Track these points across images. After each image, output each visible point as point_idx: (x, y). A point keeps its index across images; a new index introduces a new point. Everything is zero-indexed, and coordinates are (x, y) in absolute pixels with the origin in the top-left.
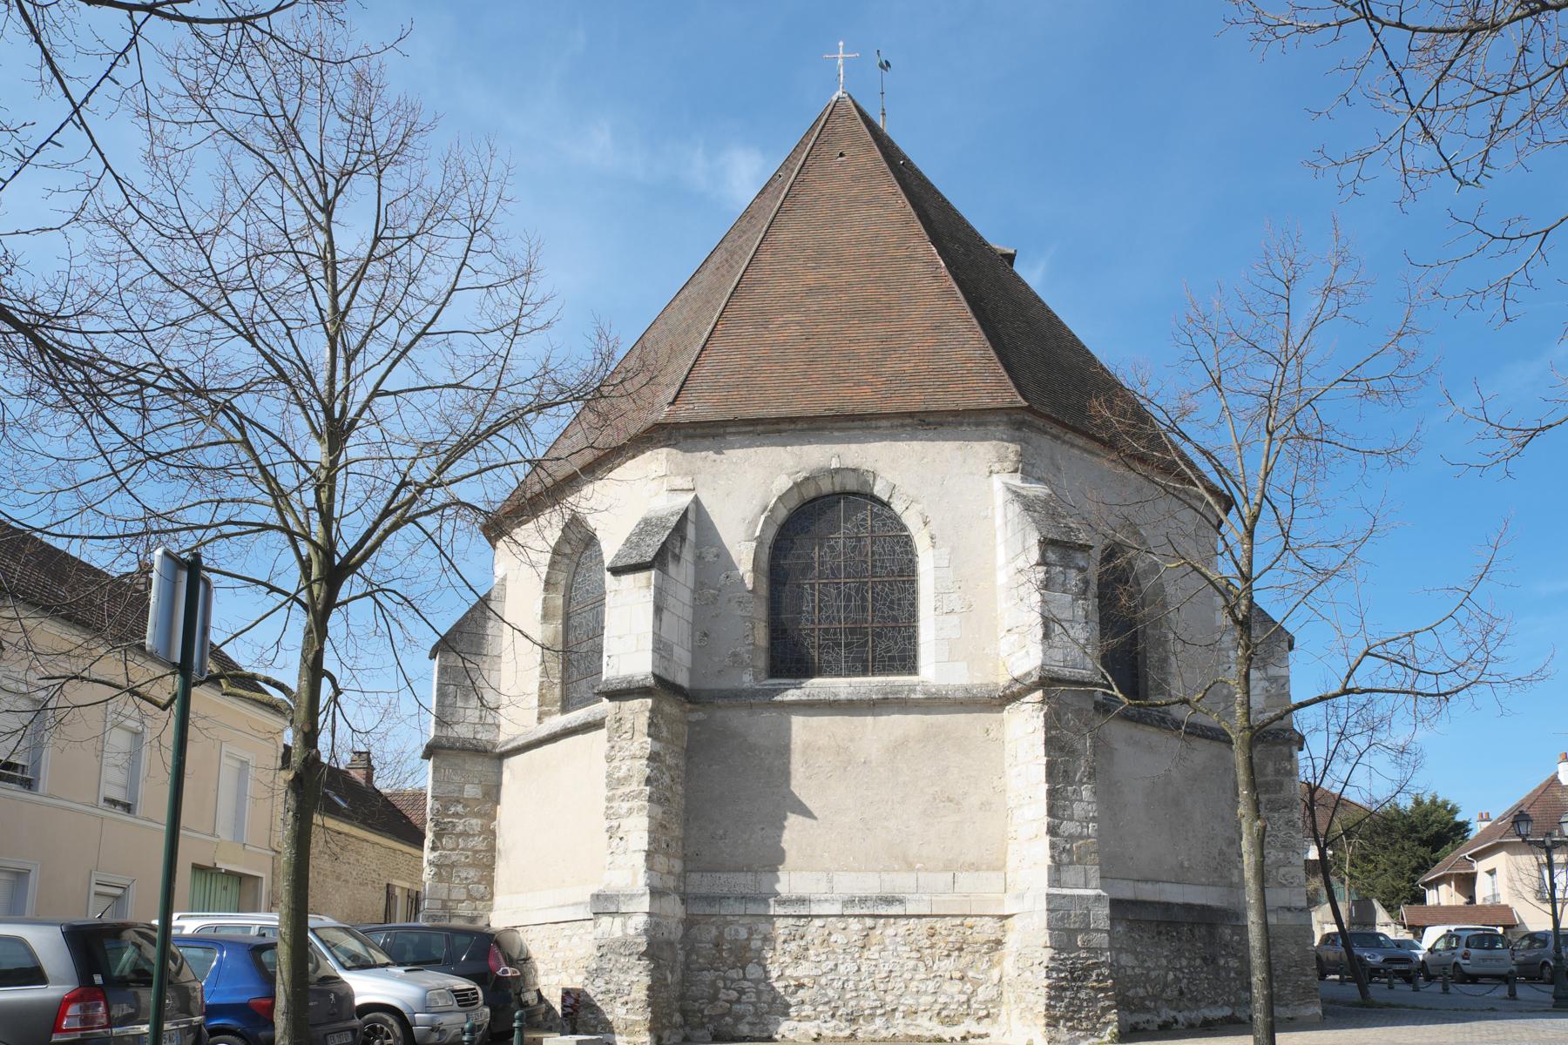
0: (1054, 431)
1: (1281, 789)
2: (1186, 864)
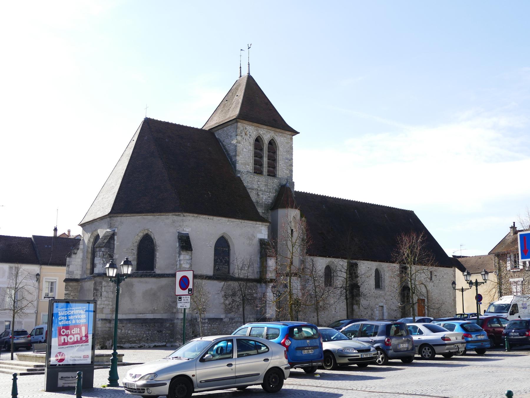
2: (156, 309)
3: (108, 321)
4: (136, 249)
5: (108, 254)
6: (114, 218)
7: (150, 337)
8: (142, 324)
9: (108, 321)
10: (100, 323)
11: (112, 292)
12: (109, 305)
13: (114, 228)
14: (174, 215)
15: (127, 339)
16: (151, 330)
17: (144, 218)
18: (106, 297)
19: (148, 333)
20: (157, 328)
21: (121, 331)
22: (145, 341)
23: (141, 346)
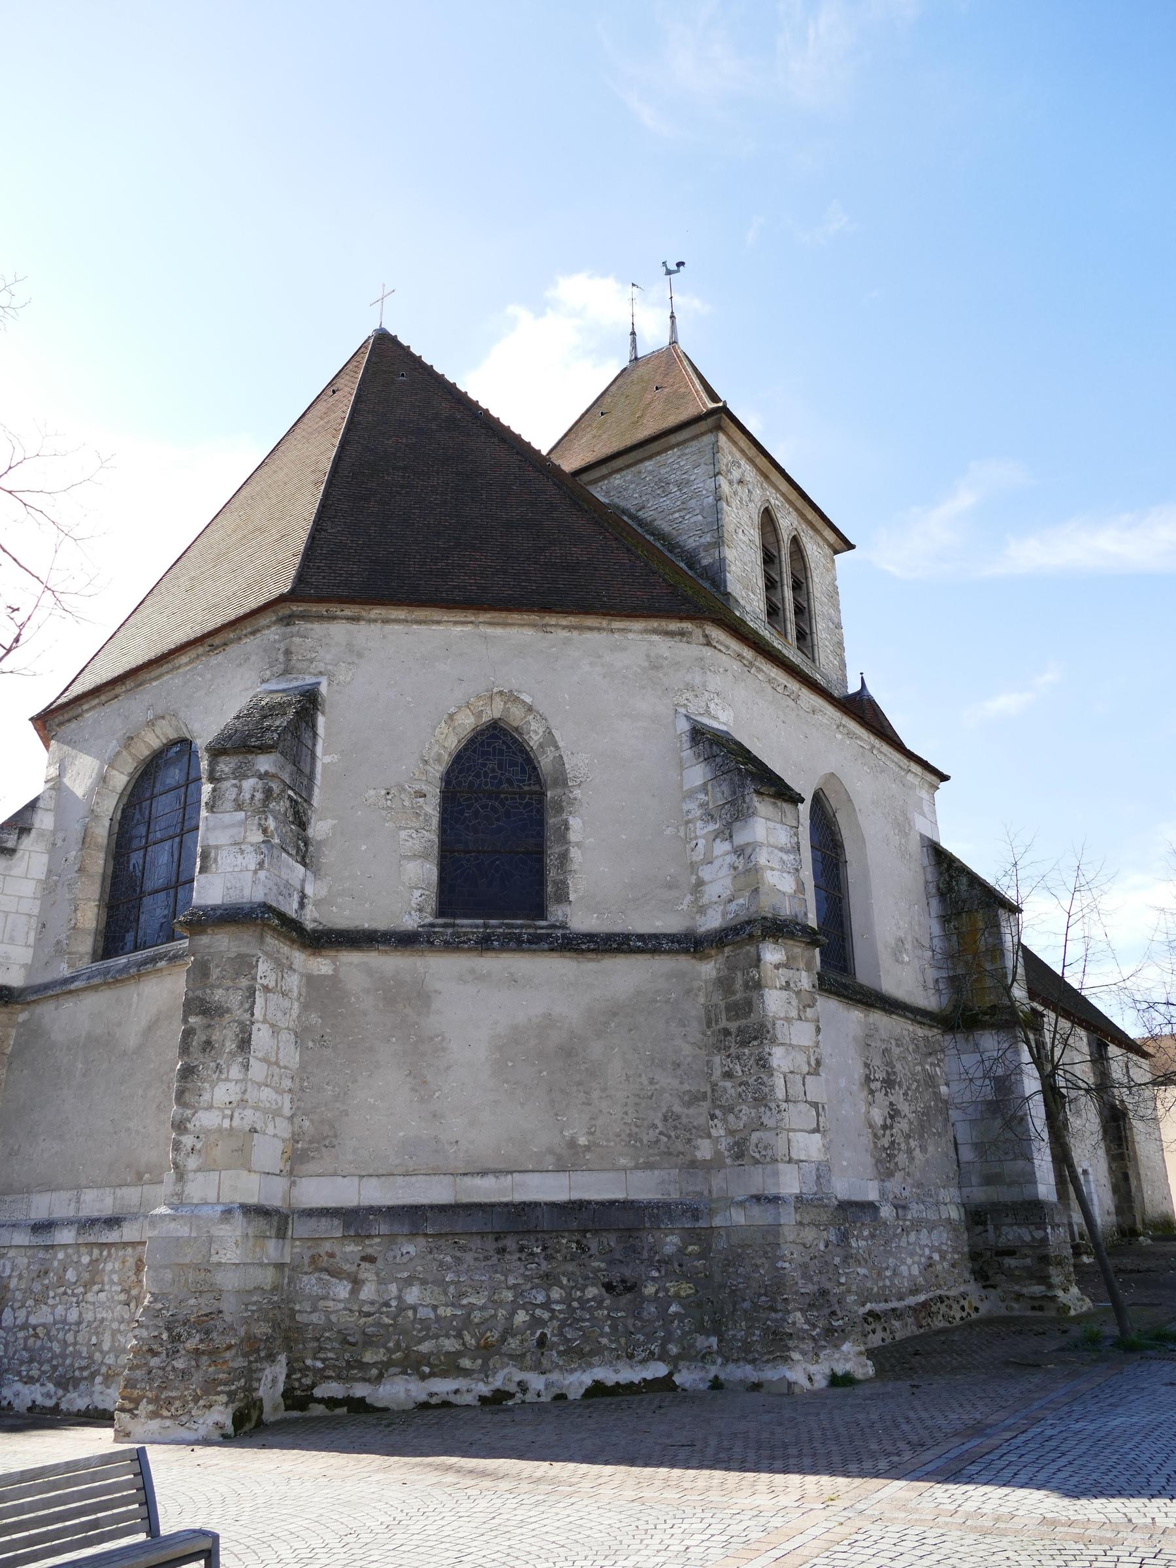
0: (348, 613)
1: (750, 1011)
2: (583, 1141)
3: (275, 1221)
4: (434, 793)
5: (290, 797)
6: (309, 626)
7: (561, 1327)
8: (496, 1239)
9: (275, 1221)
10: (238, 1233)
11: (296, 1034)
12: (277, 1113)
13: (307, 677)
14: (655, 631)
15: (398, 1344)
16: (565, 1281)
17: (485, 637)
18: (269, 1063)
19: (541, 1298)
20: (603, 1265)
21: (354, 1292)
22: (524, 1355)
23: (497, 1392)
